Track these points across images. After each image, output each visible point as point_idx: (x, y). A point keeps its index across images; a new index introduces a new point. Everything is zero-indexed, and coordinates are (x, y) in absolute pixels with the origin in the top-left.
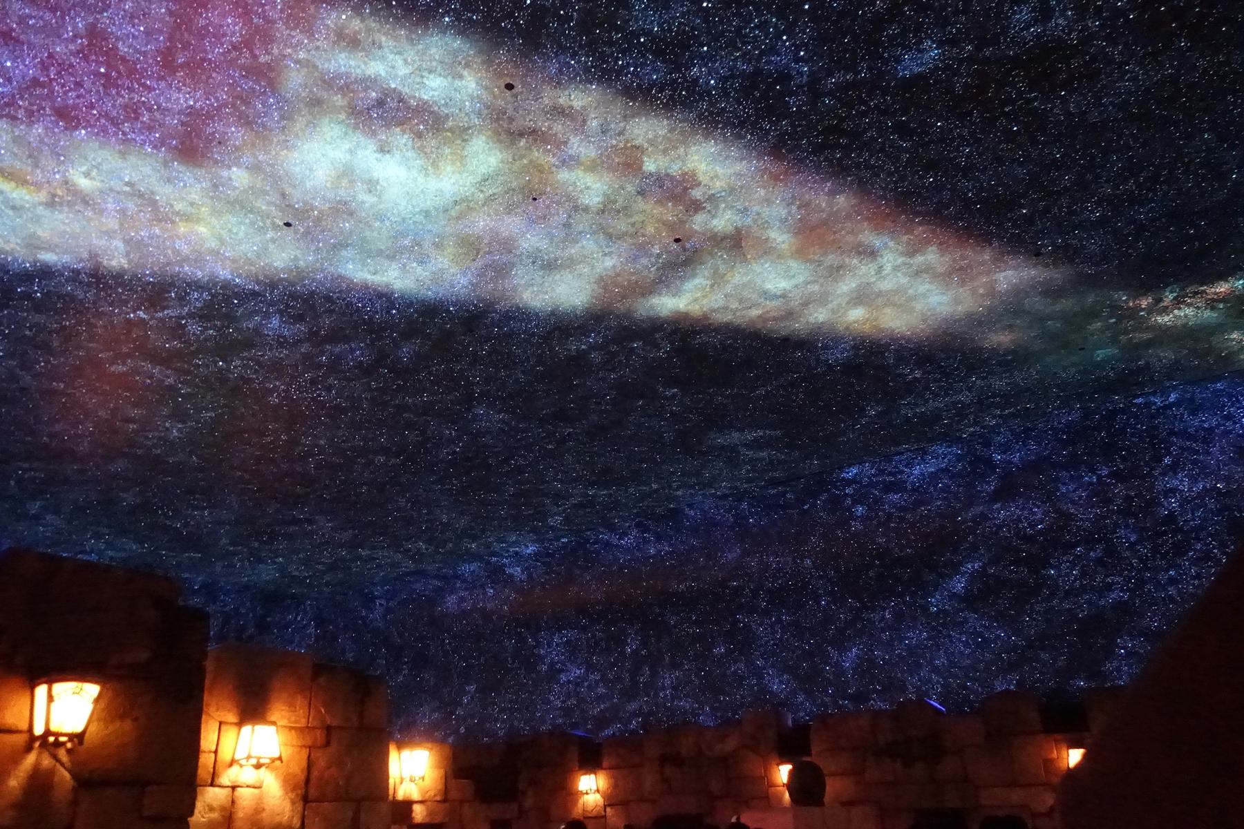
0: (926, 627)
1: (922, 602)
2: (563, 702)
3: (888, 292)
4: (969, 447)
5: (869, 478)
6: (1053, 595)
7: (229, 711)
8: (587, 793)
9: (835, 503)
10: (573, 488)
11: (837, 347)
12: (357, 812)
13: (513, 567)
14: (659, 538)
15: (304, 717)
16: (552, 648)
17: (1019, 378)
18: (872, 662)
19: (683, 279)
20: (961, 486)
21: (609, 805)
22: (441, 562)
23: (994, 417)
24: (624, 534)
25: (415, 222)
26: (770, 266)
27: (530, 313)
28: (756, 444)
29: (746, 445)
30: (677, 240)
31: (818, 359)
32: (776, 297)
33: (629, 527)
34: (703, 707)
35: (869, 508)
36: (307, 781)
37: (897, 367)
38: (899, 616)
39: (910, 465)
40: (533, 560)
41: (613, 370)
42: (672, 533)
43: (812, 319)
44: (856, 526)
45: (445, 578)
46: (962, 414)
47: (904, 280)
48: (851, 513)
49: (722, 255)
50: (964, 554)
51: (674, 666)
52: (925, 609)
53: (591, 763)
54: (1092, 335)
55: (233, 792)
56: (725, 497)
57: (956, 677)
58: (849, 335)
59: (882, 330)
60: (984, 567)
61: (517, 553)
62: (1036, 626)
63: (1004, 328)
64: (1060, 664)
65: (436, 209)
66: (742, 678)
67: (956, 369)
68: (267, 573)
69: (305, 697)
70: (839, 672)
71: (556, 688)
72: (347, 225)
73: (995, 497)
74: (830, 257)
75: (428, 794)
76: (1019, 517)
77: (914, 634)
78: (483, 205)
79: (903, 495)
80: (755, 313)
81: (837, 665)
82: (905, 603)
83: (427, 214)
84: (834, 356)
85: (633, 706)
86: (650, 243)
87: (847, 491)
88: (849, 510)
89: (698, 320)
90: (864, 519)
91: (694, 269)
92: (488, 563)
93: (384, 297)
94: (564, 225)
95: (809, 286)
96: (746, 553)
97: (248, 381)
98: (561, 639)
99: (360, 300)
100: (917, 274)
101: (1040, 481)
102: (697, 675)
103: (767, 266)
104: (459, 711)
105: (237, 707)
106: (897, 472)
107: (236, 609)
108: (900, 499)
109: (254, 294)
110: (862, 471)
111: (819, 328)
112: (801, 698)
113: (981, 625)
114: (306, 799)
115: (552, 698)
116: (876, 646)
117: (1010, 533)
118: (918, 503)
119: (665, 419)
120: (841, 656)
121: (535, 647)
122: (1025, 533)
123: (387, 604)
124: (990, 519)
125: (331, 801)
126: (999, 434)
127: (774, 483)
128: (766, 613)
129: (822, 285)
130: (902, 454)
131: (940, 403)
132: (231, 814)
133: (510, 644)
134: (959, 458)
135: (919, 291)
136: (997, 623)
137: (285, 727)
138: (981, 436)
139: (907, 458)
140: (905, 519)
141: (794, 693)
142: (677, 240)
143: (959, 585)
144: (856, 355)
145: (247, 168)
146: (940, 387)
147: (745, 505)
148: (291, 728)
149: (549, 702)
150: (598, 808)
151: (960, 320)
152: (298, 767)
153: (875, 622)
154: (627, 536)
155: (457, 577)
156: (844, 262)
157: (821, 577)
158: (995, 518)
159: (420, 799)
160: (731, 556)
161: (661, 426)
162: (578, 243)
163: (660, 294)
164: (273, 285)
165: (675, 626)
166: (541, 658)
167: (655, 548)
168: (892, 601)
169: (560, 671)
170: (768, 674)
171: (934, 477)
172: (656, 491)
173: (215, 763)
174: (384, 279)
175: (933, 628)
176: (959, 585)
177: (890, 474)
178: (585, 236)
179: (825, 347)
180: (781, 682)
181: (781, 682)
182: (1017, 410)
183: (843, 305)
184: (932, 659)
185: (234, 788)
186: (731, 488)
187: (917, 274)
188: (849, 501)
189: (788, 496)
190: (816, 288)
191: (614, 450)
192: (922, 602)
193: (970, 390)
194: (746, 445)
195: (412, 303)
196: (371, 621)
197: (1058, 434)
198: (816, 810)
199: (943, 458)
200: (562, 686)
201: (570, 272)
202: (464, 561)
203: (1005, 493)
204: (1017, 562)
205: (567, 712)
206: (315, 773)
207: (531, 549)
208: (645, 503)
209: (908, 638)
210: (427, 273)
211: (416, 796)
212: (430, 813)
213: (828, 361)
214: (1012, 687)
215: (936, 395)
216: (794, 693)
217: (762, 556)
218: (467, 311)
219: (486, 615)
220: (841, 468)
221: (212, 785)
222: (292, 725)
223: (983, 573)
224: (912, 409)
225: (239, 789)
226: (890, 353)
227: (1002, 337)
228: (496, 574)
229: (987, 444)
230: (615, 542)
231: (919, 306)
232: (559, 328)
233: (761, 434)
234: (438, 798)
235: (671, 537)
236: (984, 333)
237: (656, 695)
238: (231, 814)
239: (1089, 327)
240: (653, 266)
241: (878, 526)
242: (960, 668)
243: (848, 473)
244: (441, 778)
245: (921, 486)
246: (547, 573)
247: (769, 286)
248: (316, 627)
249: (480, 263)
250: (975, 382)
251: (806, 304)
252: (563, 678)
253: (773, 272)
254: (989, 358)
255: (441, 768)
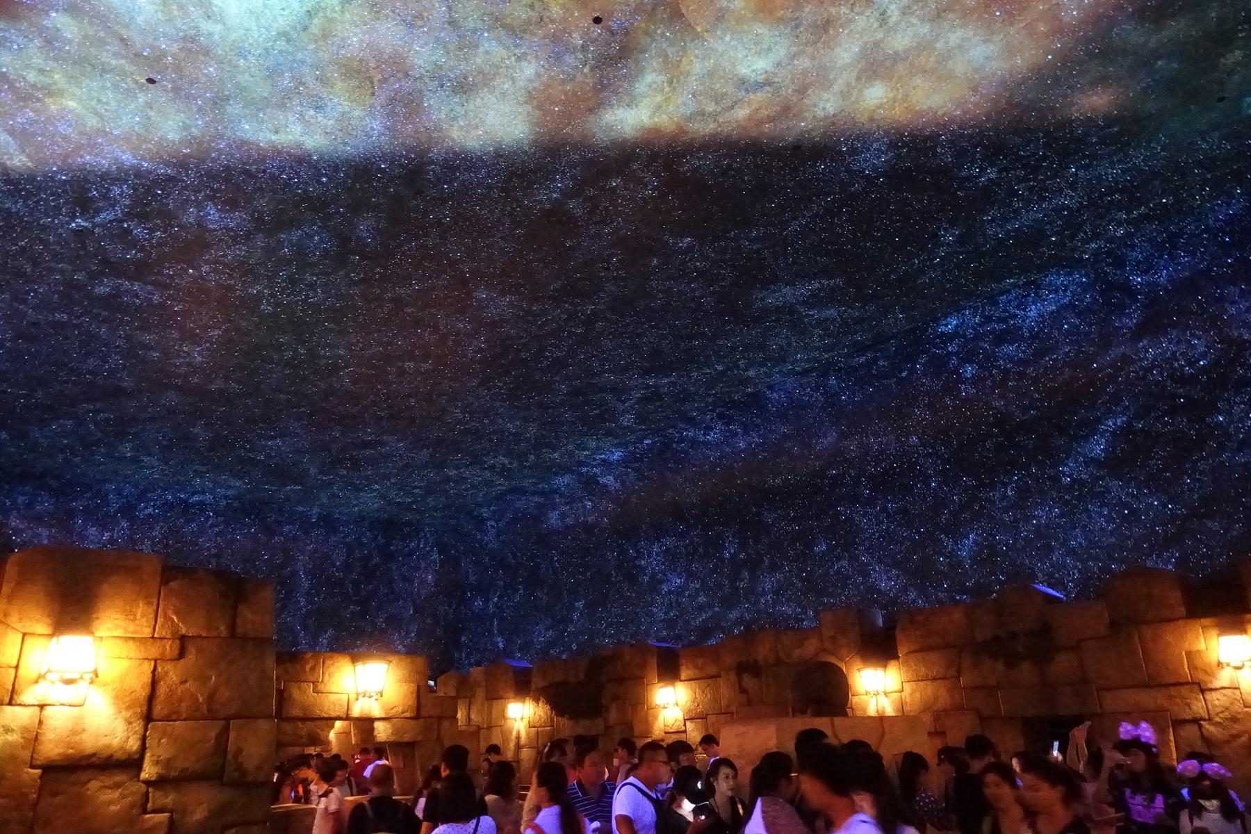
0: (1057, 502)
1: (1051, 472)
2: (666, 614)
3: (907, 51)
4: (1096, 271)
5: (974, 329)
6: (1221, 447)
7: (37, 621)
8: (665, 708)
9: (938, 365)
10: (630, 379)
11: (868, 150)
12: (223, 734)
13: (605, 476)
14: (746, 431)
15: (149, 627)
16: (652, 560)
17: (1138, 158)
18: (992, 548)
19: (632, 78)
20: (1094, 324)
21: (690, 719)
22: (532, 477)
23: (1119, 224)
24: (708, 429)
25: (281, 52)
26: (732, 39)
27: (472, 158)
28: (815, 301)
29: (804, 303)
30: (597, 20)
31: (849, 171)
32: (759, 86)
33: (712, 419)
34: (806, 611)
35: (980, 367)
36: (151, 698)
37: (960, 168)
38: (1023, 492)
39: (1022, 306)
40: (623, 467)
41: (603, 222)
42: (759, 421)
43: (820, 114)
44: (966, 390)
45: (542, 493)
46: (1072, 224)
47: (925, 29)
48: (959, 375)
49: (663, 34)
50: (1102, 410)
51: (774, 568)
52: (1056, 479)
53: (670, 672)
54: (1231, 72)
55: (41, 711)
56: (805, 373)
57: (1096, 559)
58: (878, 127)
59: (920, 114)
60: (1129, 424)
61: (604, 460)
62: (1200, 488)
63: (1094, 84)
64: (1235, 533)
65: (294, 28)
66: (848, 577)
67: (1044, 158)
68: (370, 501)
69: (149, 603)
70: (956, 563)
71: (659, 599)
72: (211, 69)
73: (1141, 331)
74: (807, 10)
75: (394, 710)
76: (1174, 353)
77: (1042, 511)
78: (343, 12)
79: (1020, 345)
80: (741, 113)
81: (952, 555)
82: (1030, 475)
83: (285, 36)
84: (874, 160)
85: (734, 615)
86: (564, 31)
87: (950, 349)
88: (956, 371)
89: (674, 137)
90: (975, 381)
91: (637, 61)
92: (581, 474)
93: (301, 161)
94: (449, 23)
95: (796, 62)
96: (842, 436)
97: (229, 288)
98: (660, 548)
99: (282, 169)
100: (939, 16)
101: (1199, 304)
102: (798, 576)
103: (728, 39)
104: (571, 628)
105: (49, 616)
106: (1008, 317)
107: (358, 539)
108: (1017, 351)
109: (172, 179)
110: (964, 320)
111: (833, 124)
112: (912, 595)
113: (1128, 493)
114: (148, 718)
115: (655, 610)
116: (997, 530)
117: (1162, 376)
118: (1039, 354)
119: (694, 280)
120: (957, 545)
121: (636, 558)
122: (1183, 373)
123: (497, 524)
124: (1134, 362)
125: (185, 720)
126: (1133, 247)
127: (860, 349)
128: (870, 502)
129: (813, 58)
130: (1009, 291)
131: (1033, 214)
132: (37, 736)
133: (612, 556)
134: (1085, 288)
135: (952, 44)
136: (1148, 488)
137: (120, 637)
138: (1109, 253)
139: (1016, 298)
140: (1025, 373)
141: (904, 590)
142: (597, 20)
143: (1098, 447)
144: (898, 157)
145: (65, 10)
146: (1031, 189)
147: (832, 381)
148: (127, 639)
149: (652, 615)
150: (678, 723)
151: (1025, 80)
152: (139, 680)
153: (995, 501)
154: (712, 430)
155: (554, 491)
156: (830, 15)
157: (930, 455)
158: (1141, 360)
159: (383, 716)
160: (829, 439)
161: (693, 290)
162: (477, 47)
163: (612, 106)
164: (183, 164)
165: (773, 524)
166: (642, 569)
167: (744, 441)
168: (1015, 475)
169: (661, 582)
170: (874, 570)
171: (1057, 316)
172: (722, 373)
173: (15, 680)
174: (290, 137)
175: (1067, 503)
176: (1098, 447)
177: (1000, 320)
178: (482, 34)
179: (853, 151)
180: (889, 579)
181: (889, 579)
182: (1150, 209)
183: (853, 83)
184: (1066, 540)
185: (42, 707)
186: (808, 361)
187: (939, 16)
188: (954, 361)
189: (881, 363)
190: (805, 63)
191: (653, 327)
192: (1051, 472)
193: (1072, 186)
194: (804, 303)
195: (337, 166)
196: (487, 544)
197: (1216, 236)
198: (845, 719)
199: (1065, 291)
200: (663, 597)
201: (491, 93)
202: (556, 474)
203: (1151, 327)
204: (1173, 411)
205: (671, 624)
206: (162, 689)
207: (617, 455)
208: (718, 389)
209: (1035, 517)
210: (331, 122)
211: (376, 711)
212: (396, 731)
213: (863, 172)
214: (1170, 567)
215: (1028, 202)
216: (904, 590)
217: (861, 438)
218: (401, 166)
219: (588, 528)
220: (936, 320)
221: (10, 704)
222: (130, 635)
223: (1127, 430)
224: (1001, 226)
225: (48, 708)
226: (943, 147)
227: (1095, 98)
228: (590, 484)
229: (1120, 263)
230: (701, 438)
231: (959, 67)
232: (513, 174)
233: (817, 285)
234: (407, 715)
235: (757, 426)
236: (1065, 96)
237: (757, 602)
238: (37, 736)
239: (1222, 60)
240: (584, 66)
241: (993, 388)
242: (1100, 548)
243: (946, 325)
244: (412, 693)
245: (1041, 330)
246: (639, 480)
247: (744, 71)
248: (440, 553)
249: (382, 98)
250: (1076, 174)
251: (802, 91)
252: (665, 588)
253: (740, 48)
254: (1087, 134)
255: (411, 682)
